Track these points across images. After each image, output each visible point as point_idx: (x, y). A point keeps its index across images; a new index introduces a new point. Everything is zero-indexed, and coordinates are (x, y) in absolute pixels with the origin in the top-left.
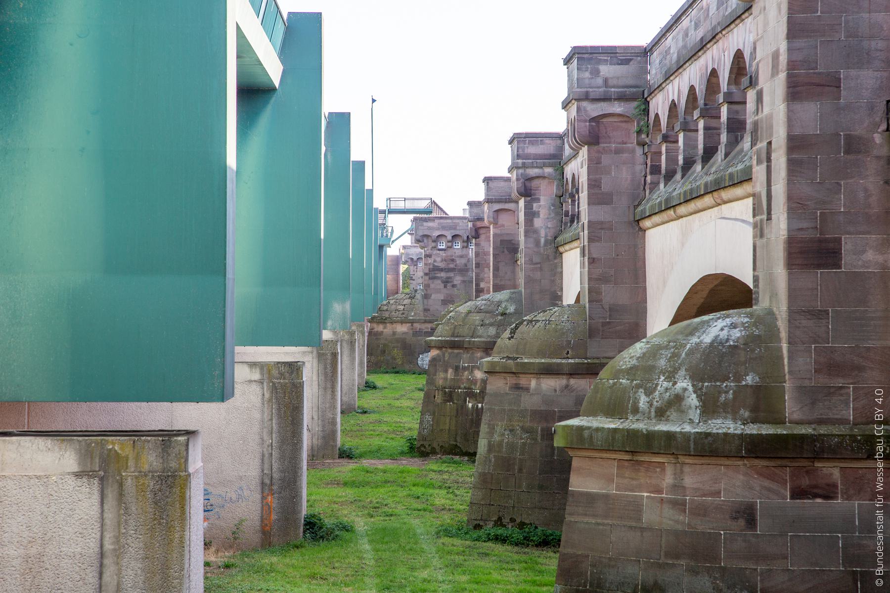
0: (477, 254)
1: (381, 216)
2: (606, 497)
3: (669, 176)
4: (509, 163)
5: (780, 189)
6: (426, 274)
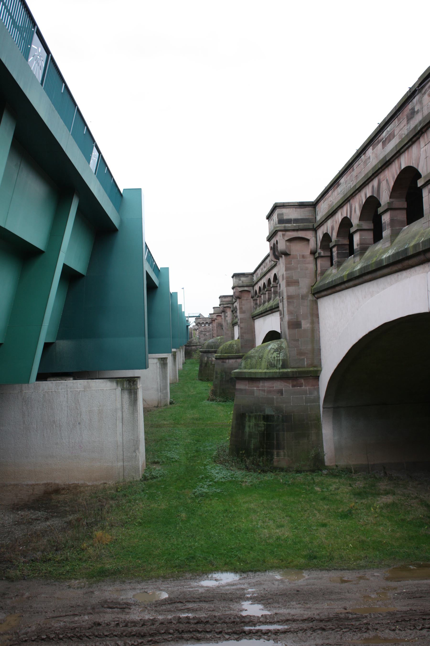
0: (212, 327)
1: (187, 318)
2: (245, 389)
3: (260, 306)
4: (219, 303)
5: (285, 309)
6: (199, 333)
